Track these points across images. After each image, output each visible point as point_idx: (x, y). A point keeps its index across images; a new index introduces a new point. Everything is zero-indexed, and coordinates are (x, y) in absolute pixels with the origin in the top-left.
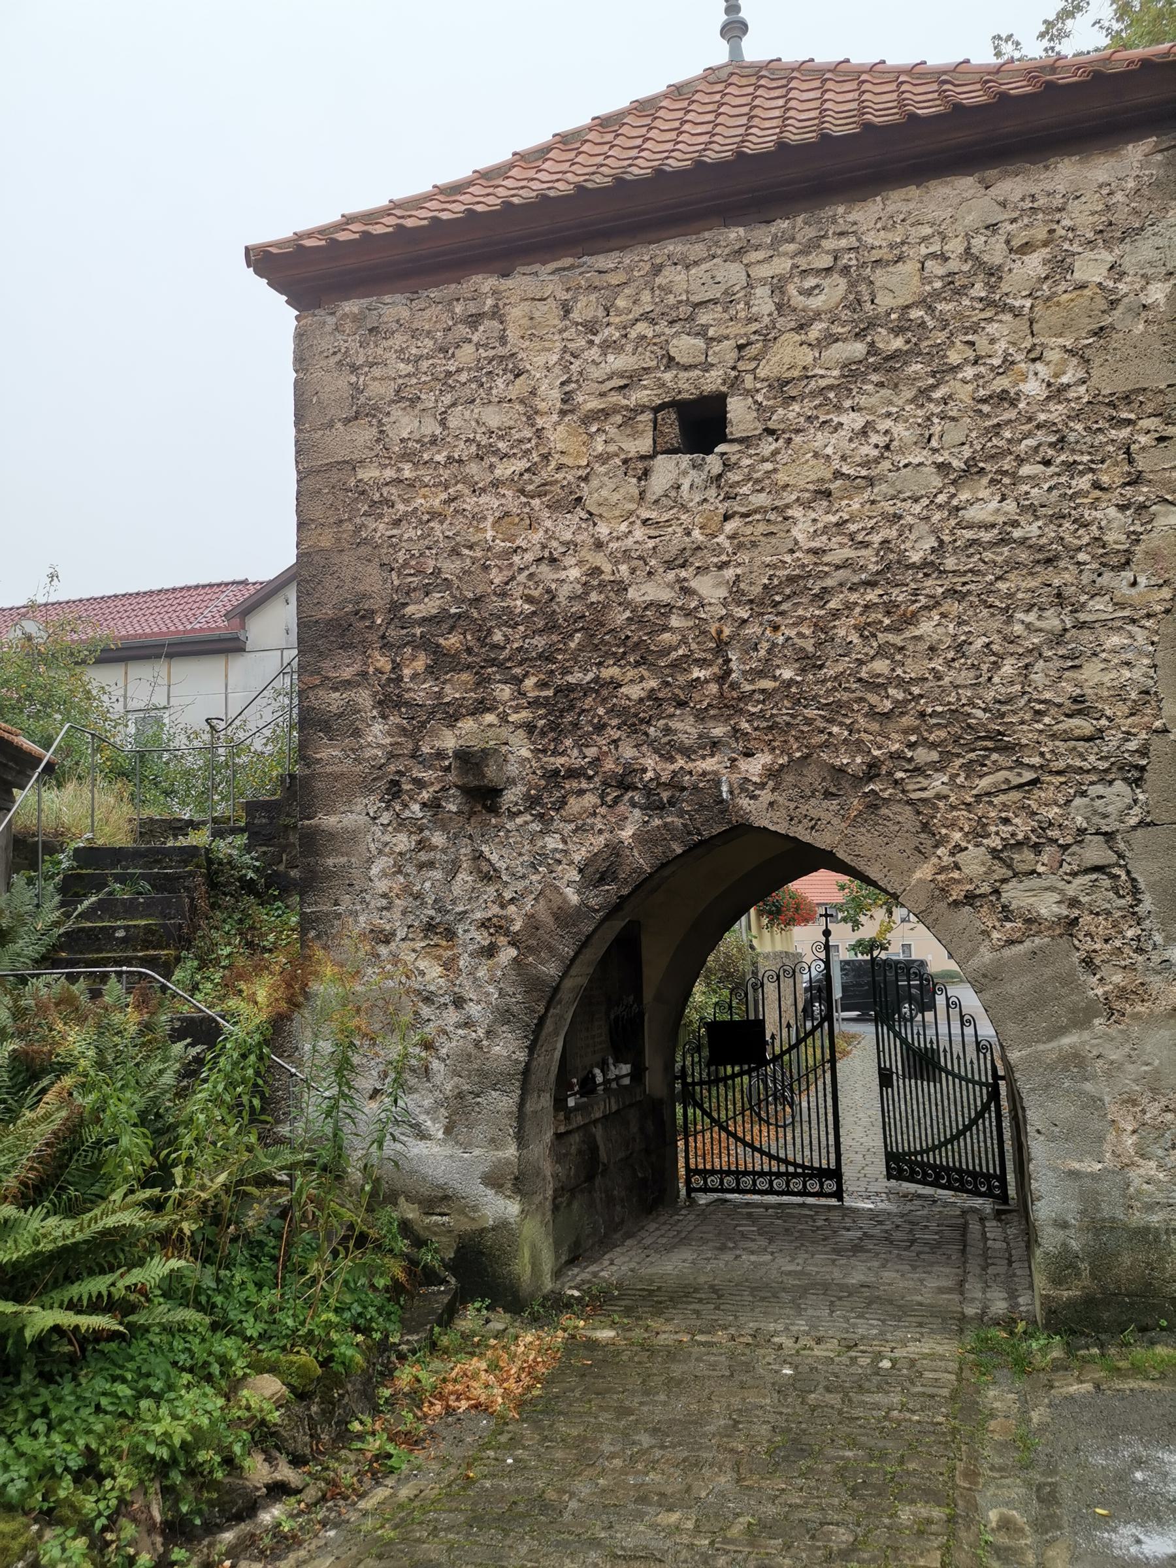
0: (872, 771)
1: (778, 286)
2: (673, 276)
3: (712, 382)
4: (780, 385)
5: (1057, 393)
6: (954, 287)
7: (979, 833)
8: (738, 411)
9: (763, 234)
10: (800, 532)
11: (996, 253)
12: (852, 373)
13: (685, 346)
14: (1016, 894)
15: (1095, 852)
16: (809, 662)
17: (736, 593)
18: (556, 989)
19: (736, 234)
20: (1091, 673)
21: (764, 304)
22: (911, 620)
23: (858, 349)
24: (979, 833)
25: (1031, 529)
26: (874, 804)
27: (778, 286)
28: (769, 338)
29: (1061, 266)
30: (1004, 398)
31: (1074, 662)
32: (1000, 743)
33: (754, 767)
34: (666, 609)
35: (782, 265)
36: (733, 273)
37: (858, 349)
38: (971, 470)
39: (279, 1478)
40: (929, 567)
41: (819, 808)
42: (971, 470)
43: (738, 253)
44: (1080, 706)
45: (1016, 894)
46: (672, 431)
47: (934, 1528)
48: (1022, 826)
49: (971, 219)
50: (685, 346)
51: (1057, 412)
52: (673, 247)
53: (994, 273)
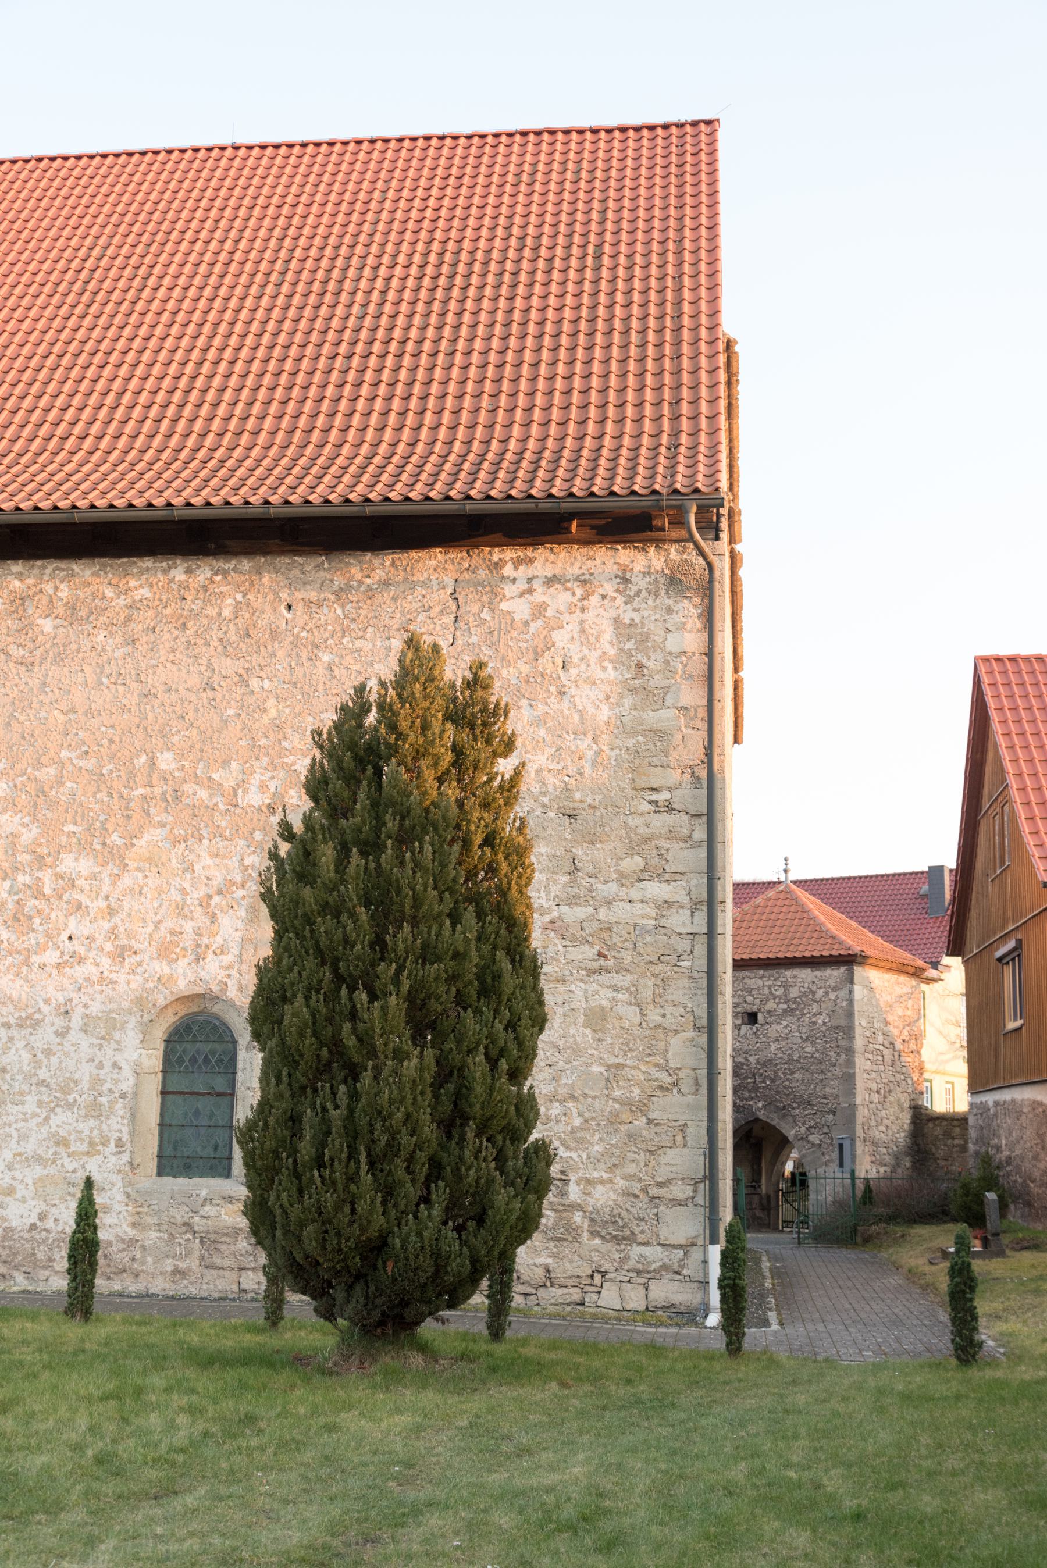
0: (784, 1108)
1: (769, 987)
2: (747, 980)
3: (755, 1009)
4: (769, 1012)
5: (824, 1023)
6: (804, 994)
7: (804, 1123)
8: (760, 1016)
9: (767, 974)
10: (773, 1048)
11: (814, 989)
12: (785, 1011)
13: (749, 999)
14: (811, 1138)
15: (826, 1130)
16: (773, 1081)
17: (758, 1062)
18: (475, 769)
19: (761, 972)
20: (827, 1089)
21: (766, 992)
22: (793, 1073)
23: (785, 1006)
24: (804, 1123)
25: (817, 1055)
26: (784, 1115)
27: (769, 987)
28: (767, 999)
29: (827, 993)
30: (815, 1023)
31: (824, 1086)
32: (809, 1103)
33: (760, 1105)
34: (743, 1064)
35: (770, 983)
36: (760, 983)
37: (785, 1006)
38: (807, 1040)
39: (65, 1253)
40: (798, 1061)
41: (774, 1115)
42: (807, 1040)
43: (761, 978)
44: (825, 1097)
45: (811, 1138)
46: (746, 1020)
47: (372, 865)
48: (812, 1123)
49: (810, 979)
50: (749, 999)
51: (824, 1028)
52: (747, 973)
53: (814, 993)
